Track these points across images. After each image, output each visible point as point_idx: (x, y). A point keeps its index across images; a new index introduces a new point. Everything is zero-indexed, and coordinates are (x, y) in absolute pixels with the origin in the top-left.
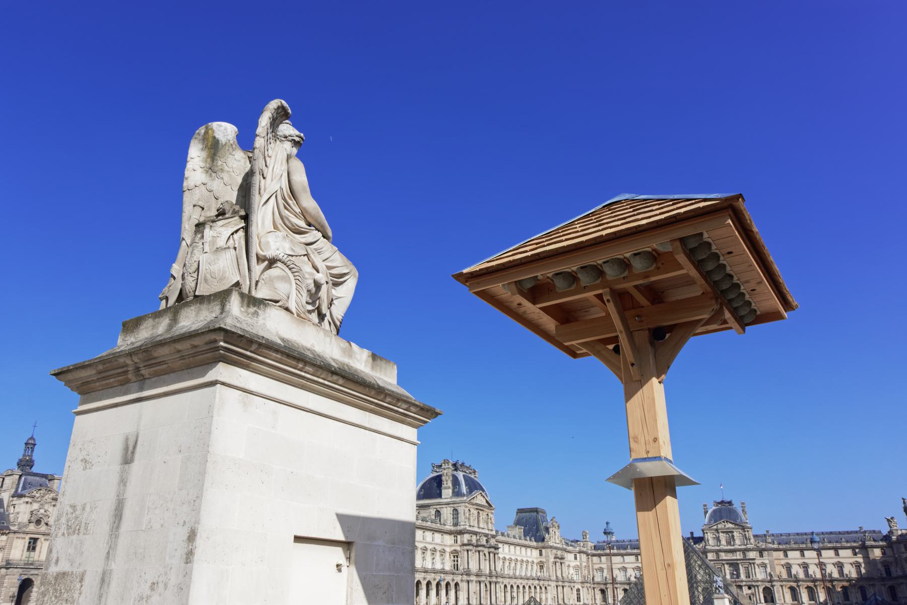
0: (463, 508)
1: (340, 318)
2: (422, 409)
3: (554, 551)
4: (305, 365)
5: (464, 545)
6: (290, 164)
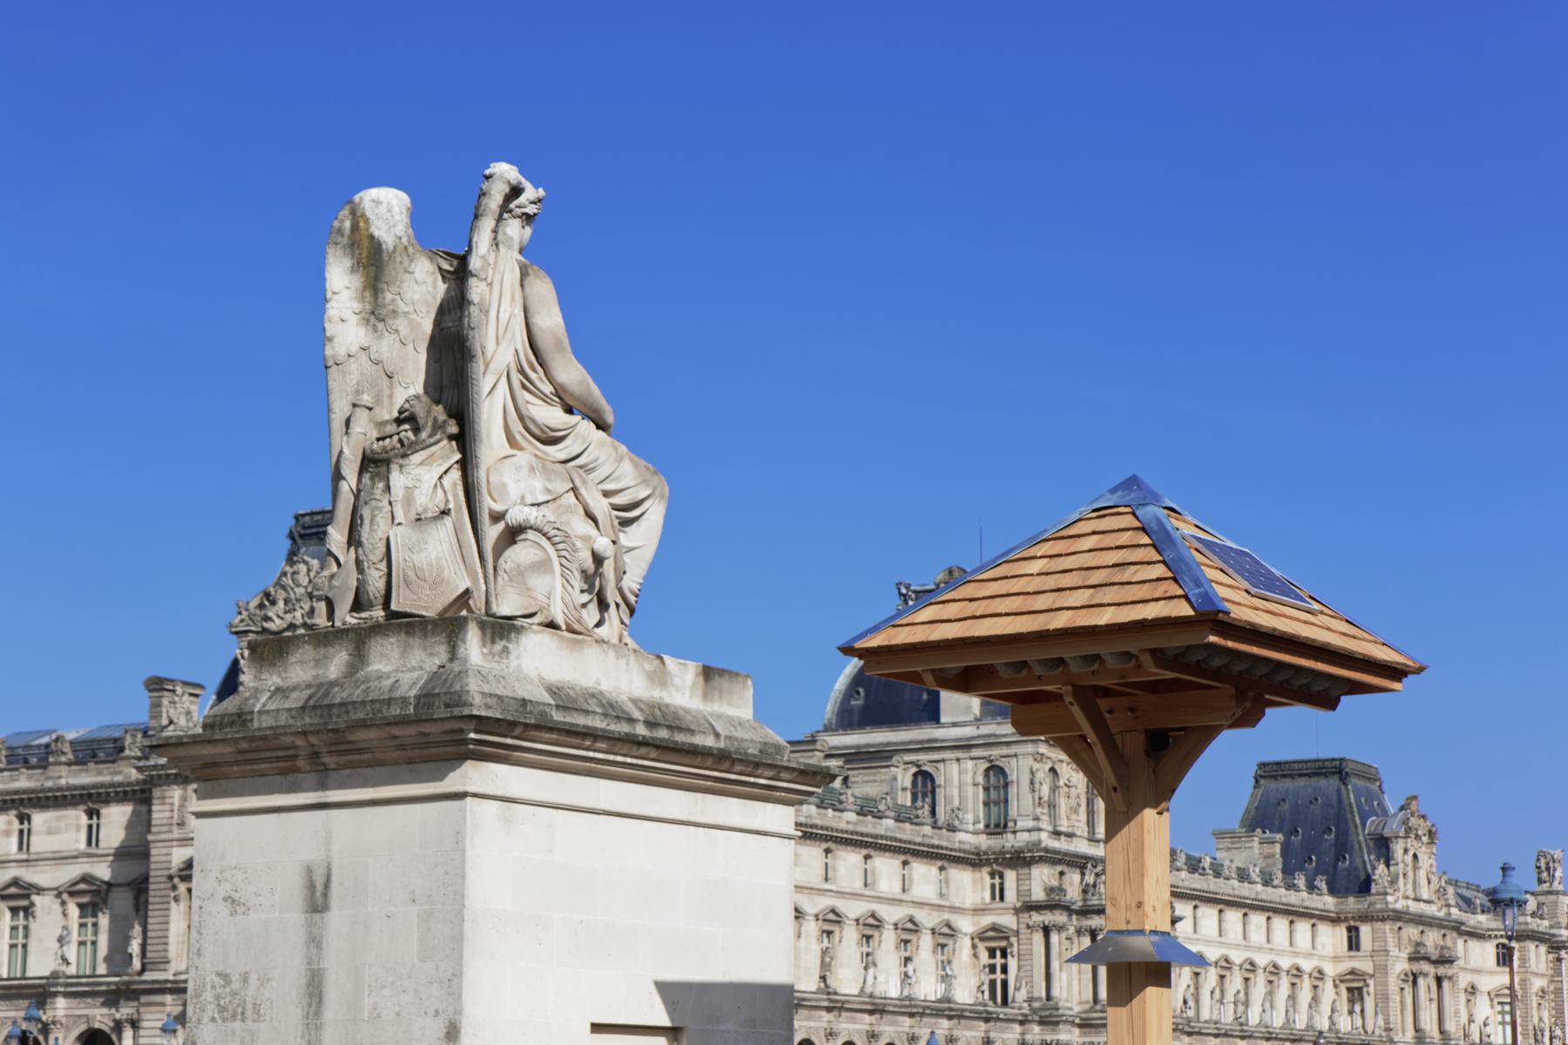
0: (1026, 763)
1: (635, 587)
3: (1412, 932)
5: (1031, 907)
6: (528, 289)
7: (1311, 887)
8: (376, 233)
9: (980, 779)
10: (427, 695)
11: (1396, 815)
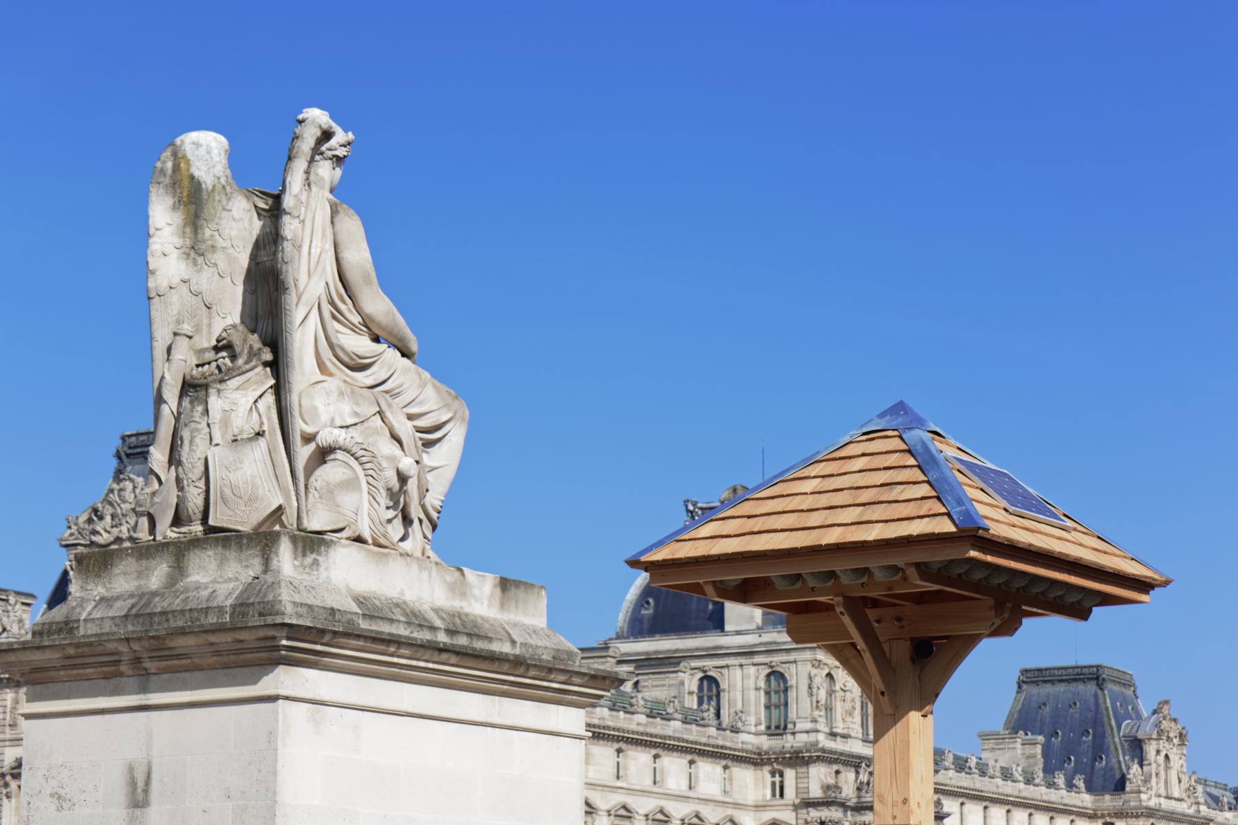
0: (805, 669)
1: (438, 504)
2: (593, 677)
4: (399, 648)
6: (338, 227)
7: (1070, 786)
8: (196, 174)
9: (762, 684)
10: (242, 605)
11: (1149, 718)
